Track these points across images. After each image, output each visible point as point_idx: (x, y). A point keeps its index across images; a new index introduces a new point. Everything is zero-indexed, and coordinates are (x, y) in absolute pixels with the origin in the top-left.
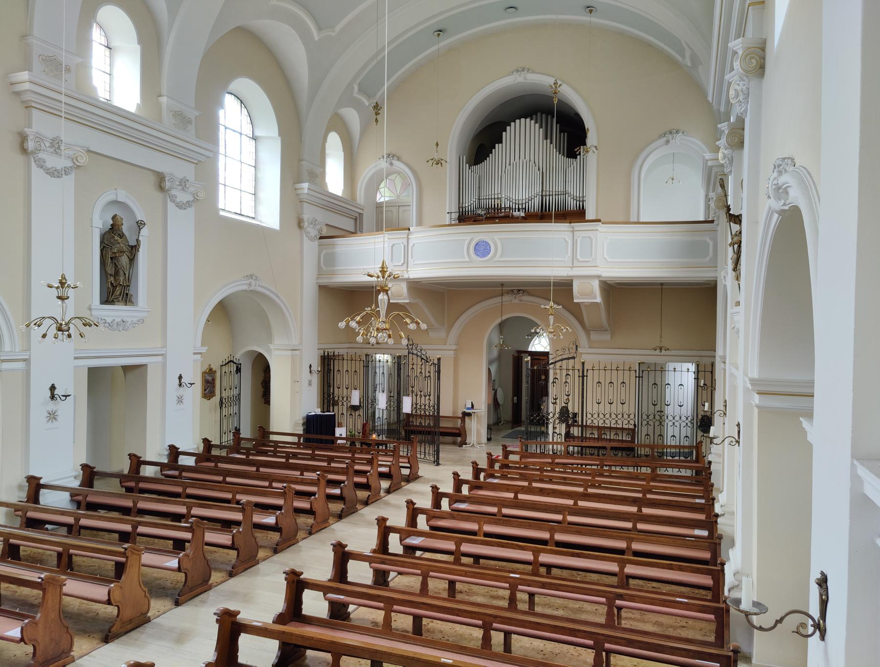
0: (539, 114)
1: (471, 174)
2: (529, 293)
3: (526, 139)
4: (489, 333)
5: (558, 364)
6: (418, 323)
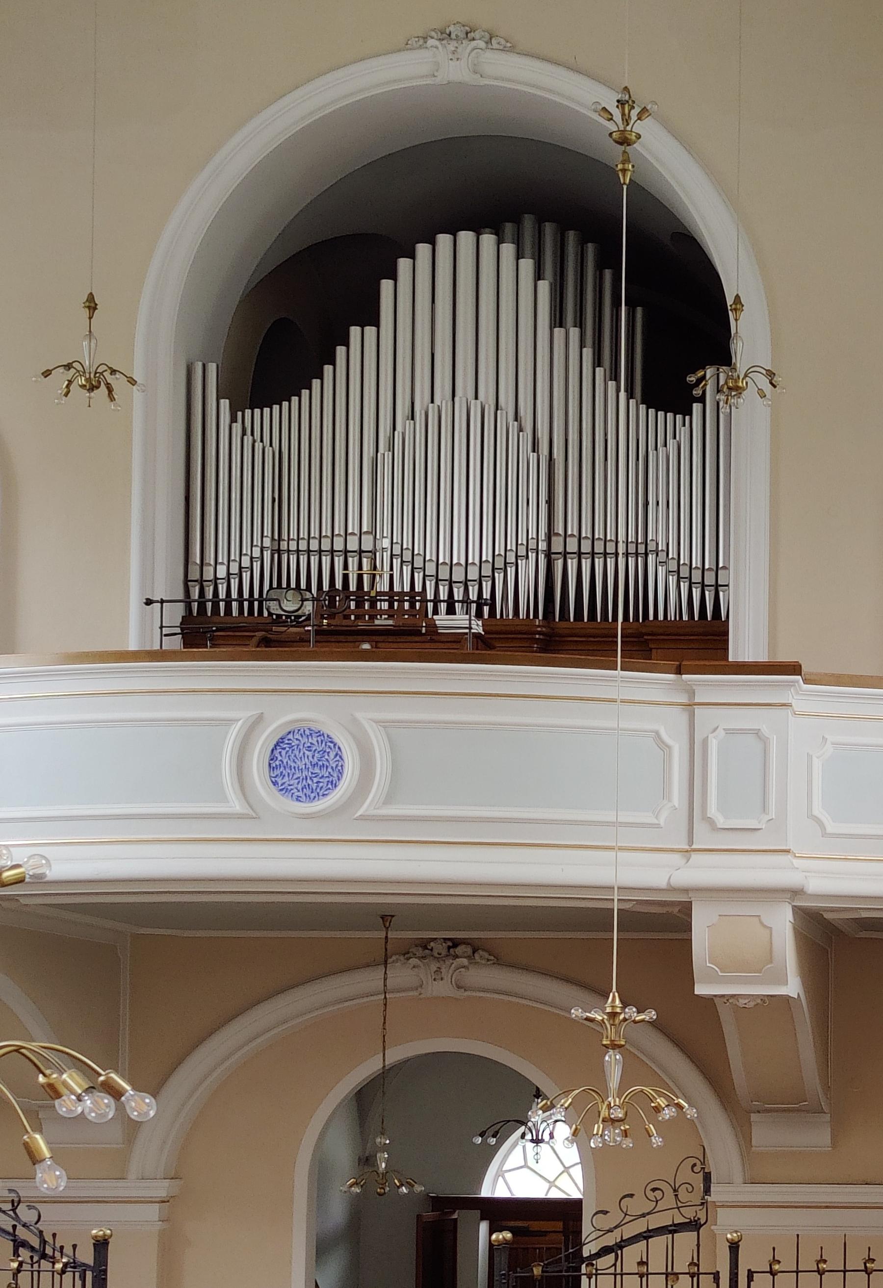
0: (528, 222)
1: (241, 442)
2: (498, 958)
3: (469, 319)
4: (314, 1131)
5: (632, 1255)
6: (116, 1093)
